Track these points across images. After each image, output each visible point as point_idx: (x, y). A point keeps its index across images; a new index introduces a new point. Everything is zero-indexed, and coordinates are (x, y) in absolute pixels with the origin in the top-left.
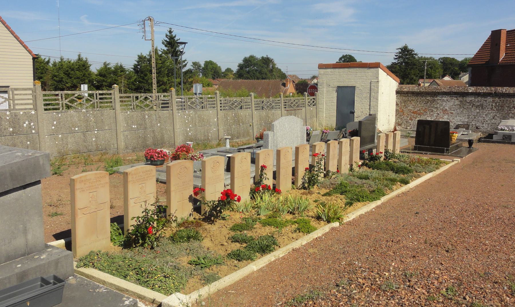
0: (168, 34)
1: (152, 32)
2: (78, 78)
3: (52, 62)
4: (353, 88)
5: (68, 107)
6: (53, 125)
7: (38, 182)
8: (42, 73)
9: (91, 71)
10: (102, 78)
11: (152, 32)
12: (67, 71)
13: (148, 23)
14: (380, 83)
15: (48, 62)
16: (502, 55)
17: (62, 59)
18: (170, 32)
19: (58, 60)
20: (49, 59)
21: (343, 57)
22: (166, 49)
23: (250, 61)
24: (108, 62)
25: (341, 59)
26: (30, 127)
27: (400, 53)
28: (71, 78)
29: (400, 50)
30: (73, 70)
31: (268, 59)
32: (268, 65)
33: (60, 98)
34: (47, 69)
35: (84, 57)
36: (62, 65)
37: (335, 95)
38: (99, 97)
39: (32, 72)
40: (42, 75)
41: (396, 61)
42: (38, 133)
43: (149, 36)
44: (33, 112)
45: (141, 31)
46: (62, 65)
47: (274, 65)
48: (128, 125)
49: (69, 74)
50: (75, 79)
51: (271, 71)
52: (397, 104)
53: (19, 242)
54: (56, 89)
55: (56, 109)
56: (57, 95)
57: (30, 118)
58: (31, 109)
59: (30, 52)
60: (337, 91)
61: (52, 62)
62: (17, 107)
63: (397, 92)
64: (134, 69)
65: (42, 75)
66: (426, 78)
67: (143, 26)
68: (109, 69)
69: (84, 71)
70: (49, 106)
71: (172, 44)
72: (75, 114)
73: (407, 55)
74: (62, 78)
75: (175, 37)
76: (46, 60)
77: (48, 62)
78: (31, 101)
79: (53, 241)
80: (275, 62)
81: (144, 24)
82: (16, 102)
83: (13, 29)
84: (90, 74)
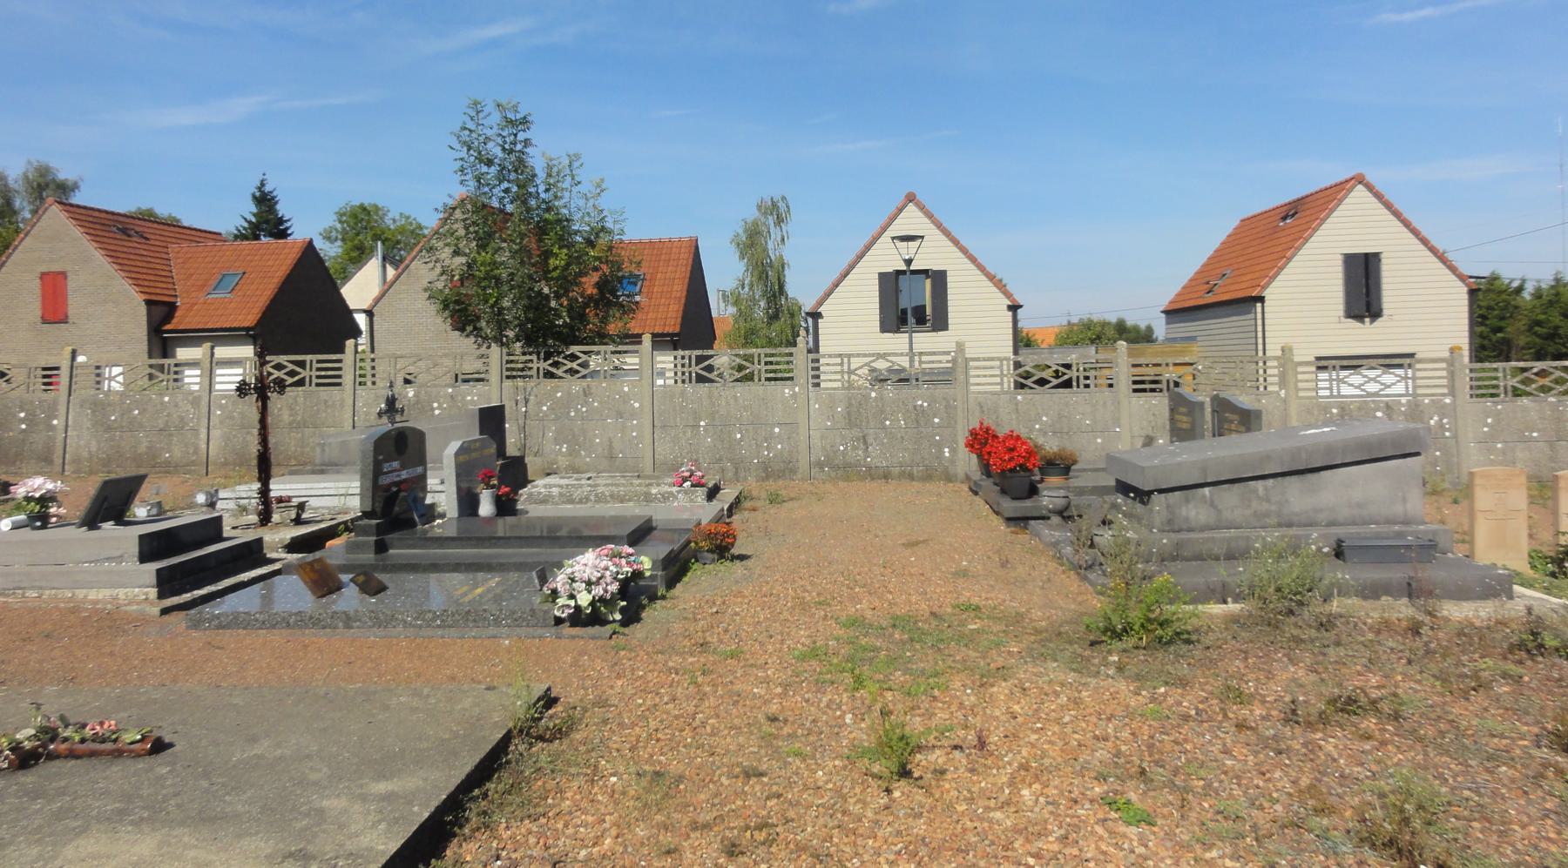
3: (1530, 288)
5: (1517, 393)
6: (1487, 425)
7: (1417, 454)
8: (1502, 318)
15: (1520, 290)
20: (1524, 281)
26: (1441, 426)
33: (1500, 375)
34: (1516, 307)
36: (1557, 294)
38: (315, 365)
39: (1466, 321)
40: (1502, 324)
42: (1455, 436)
44: (1448, 401)
46: (1557, 294)
53: (1398, 509)
54: (1539, 357)
55: (1493, 395)
56: (1496, 370)
57: (1443, 411)
58: (1444, 395)
59: (1462, 278)
61: (1530, 288)
62: (1420, 391)
65: (1502, 324)
70: (1485, 390)
72: (1532, 405)
74: (1557, 328)
76: (1515, 284)
77: (1520, 290)
78: (1444, 382)
82: (1419, 382)
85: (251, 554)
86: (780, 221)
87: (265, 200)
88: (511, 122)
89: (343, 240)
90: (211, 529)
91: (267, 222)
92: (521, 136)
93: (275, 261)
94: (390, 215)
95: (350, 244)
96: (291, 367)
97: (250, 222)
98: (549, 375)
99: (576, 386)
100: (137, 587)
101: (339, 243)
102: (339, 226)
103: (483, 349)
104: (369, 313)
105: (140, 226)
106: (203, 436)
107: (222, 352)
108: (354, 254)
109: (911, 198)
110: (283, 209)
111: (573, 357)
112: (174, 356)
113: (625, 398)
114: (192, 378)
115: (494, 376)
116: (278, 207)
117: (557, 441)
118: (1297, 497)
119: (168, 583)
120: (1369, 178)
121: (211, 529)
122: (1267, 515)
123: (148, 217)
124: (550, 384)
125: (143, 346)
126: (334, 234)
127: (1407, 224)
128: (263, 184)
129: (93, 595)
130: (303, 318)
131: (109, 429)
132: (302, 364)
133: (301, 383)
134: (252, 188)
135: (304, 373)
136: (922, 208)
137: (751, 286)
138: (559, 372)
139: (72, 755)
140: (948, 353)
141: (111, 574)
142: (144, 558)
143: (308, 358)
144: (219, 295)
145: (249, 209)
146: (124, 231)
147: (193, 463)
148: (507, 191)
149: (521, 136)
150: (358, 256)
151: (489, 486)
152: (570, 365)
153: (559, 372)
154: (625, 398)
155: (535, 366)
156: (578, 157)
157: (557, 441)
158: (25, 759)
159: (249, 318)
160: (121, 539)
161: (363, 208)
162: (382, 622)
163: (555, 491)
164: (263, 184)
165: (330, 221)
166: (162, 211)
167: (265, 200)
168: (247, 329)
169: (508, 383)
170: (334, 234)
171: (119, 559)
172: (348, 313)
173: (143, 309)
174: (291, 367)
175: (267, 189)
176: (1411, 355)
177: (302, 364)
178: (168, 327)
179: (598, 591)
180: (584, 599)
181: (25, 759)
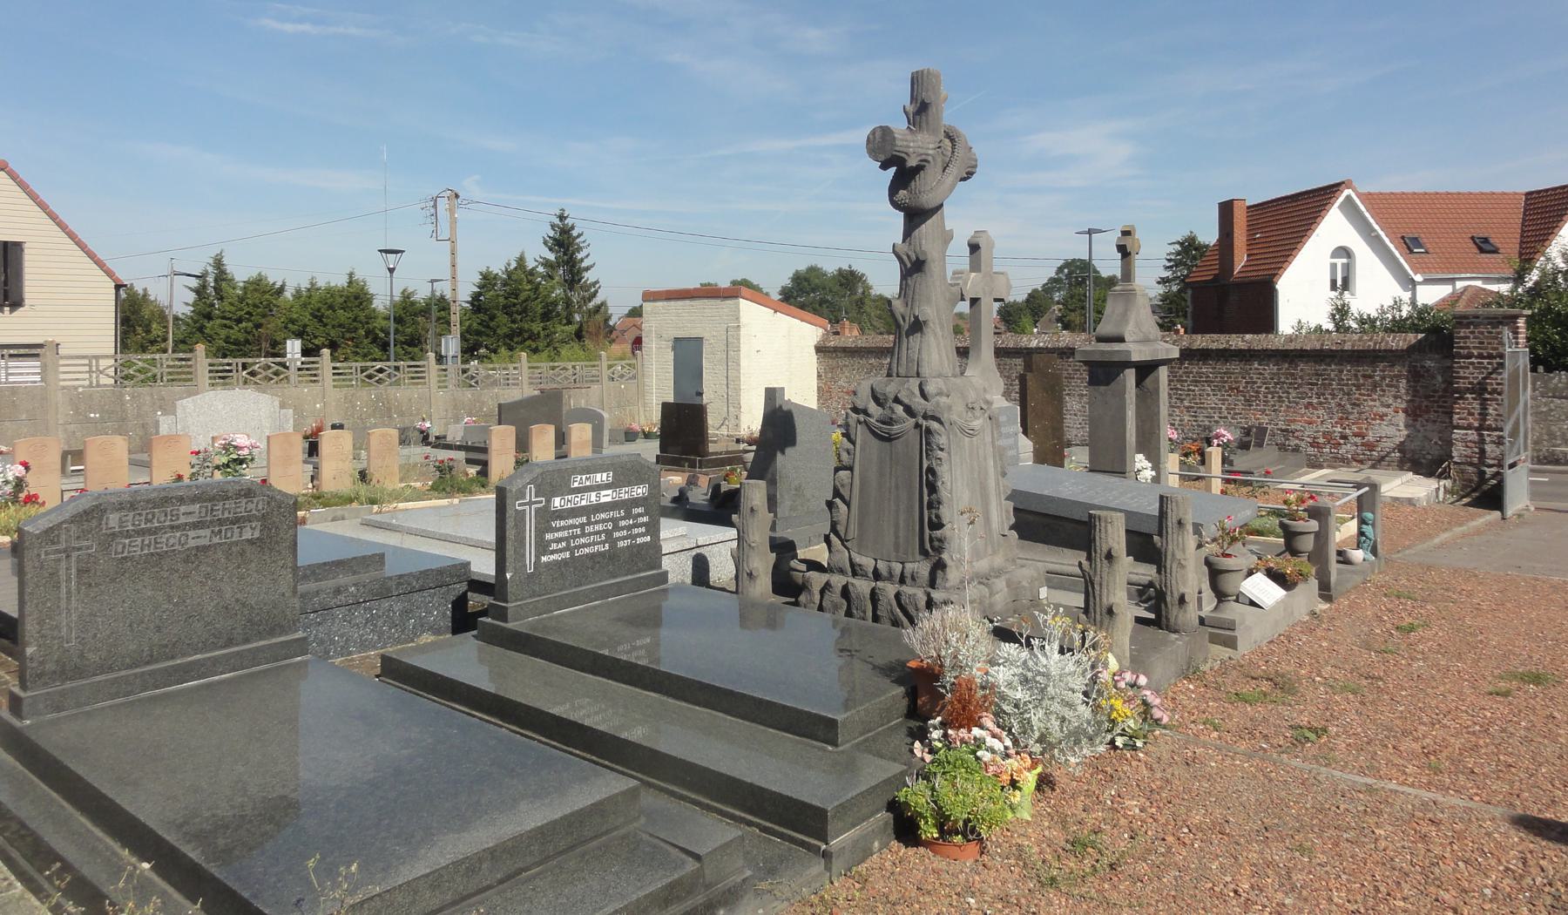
0: (557, 221)
1: (454, 222)
2: (340, 326)
4: (699, 340)
8: (264, 316)
11: (454, 222)
13: (443, 205)
14: (743, 331)
15: (281, 290)
16: (1240, 261)
18: (562, 218)
19: (305, 285)
21: (1068, 264)
22: (552, 257)
23: (806, 280)
24: (410, 290)
25: (1060, 270)
27: (1178, 253)
29: (1178, 247)
30: (331, 307)
31: (852, 273)
32: (853, 291)
35: (358, 276)
37: (671, 356)
40: (263, 321)
41: (1168, 274)
43: (445, 233)
47: (868, 288)
48: (77, 412)
51: (860, 303)
52: (819, 376)
59: (110, 273)
60: (674, 349)
63: (820, 349)
64: (472, 303)
65: (263, 321)
68: (413, 304)
69: (356, 310)
71: (564, 242)
73: (1194, 258)
74: (305, 326)
75: (573, 228)
77: (281, 290)
80: (870, 282)
81: (435, 206)
84: (372, 316)
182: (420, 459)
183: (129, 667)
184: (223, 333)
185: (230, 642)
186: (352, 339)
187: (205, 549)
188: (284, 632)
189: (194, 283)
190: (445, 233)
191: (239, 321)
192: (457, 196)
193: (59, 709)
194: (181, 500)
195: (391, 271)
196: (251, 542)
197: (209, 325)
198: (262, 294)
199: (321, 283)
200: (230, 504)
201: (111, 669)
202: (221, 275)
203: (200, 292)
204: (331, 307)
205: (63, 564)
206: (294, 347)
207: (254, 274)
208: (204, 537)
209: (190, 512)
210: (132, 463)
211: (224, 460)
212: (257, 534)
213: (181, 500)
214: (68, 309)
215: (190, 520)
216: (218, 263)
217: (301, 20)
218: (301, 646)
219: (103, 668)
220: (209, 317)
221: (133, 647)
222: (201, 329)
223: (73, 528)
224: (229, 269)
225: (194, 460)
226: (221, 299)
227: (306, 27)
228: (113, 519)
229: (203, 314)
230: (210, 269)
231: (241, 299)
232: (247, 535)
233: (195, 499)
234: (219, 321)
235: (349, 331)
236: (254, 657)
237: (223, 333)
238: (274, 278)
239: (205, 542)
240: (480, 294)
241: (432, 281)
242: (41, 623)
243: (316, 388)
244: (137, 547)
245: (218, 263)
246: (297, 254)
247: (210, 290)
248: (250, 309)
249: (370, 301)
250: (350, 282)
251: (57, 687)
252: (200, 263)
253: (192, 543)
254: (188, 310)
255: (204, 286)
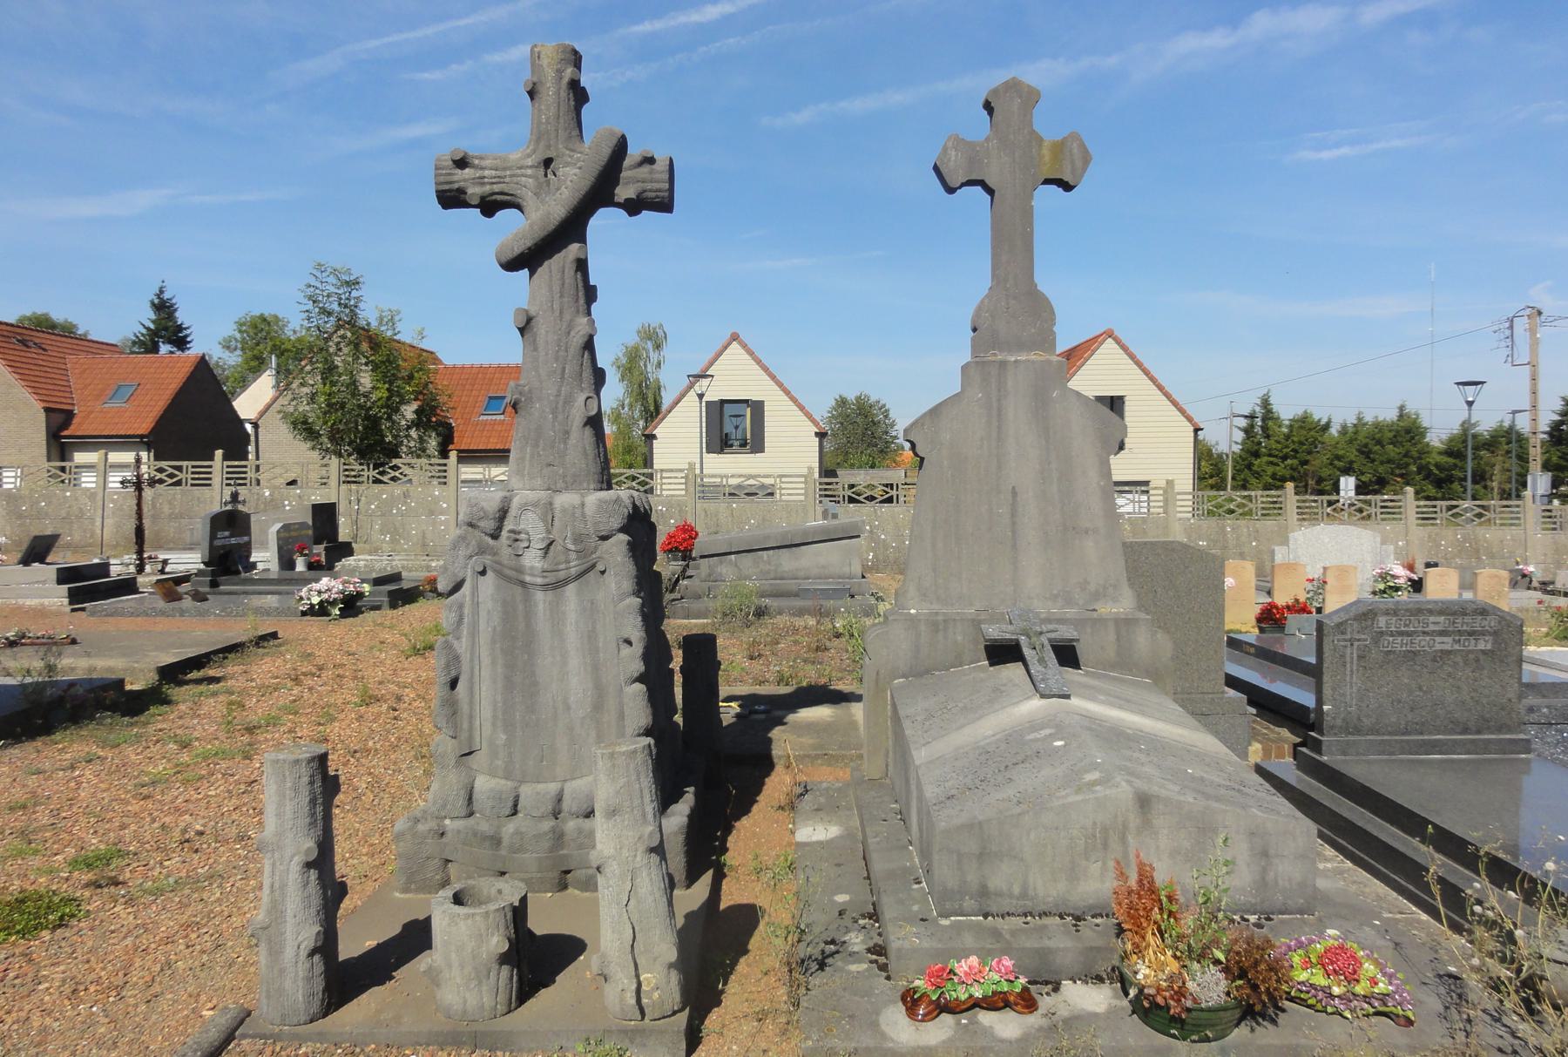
1: (1534, 344)
2: (1389, 461)
8: (1310, 453)
9: (1428, 445)
10: (1451, 460)
12: (1366, 445)
13: (1521, 325)
15: (1327, 426)
17: (1360, 419)
19: (1351, 420)
28: (1373, 461)
30: (1379, 442)
35: (1411, 408)
45: (1503, 344)
49: (1370, 451)
50: (1382, 463)
53: (846, 570)
59: (1189, 419)
64: (1549, 433)
66: (1234, 488)
67: (1508, 333)
74: (1351, 462)
76: (1323, 422)
77: (1327, 426)
79: (1029, 698)
81: (1511, 327)
83: (1161, 381)
84: (1426, 450)
85: (127, 586)
86: (658, 347)
87: (163, 308)
88: (347, 283)
89: (243, 349)
90: (103, 569)
91: (166, 329)
92: (354, 294)
93: (171, 368)
94: (291, 326)
95: (249, 354)
96: (171, 470)
97: (148, 329)
98: (377, 481)
99: (397, 489)
100: (58, 598)
101: (239, 352)
102: (238, 336)
103: (326, 461)
104: (256, 426)
105: (40, 338)
106: (98, 523)
107: (116, 457)
108: (253, 364)
109: (735, 337)
110: (182, 317)
111: (395, 468)
112: (71, 460)
113: (436, 500)
114: (88, 480)
115: (333, 482)
116: (177, 314)
117: (382, 532)
118: (787, 562)
119: (76, 597)
120: (1116, 333)
121: (103, 569)
122: (768, 572)
123: (44, 325)
124: (377, 488)
125: (42, 450)
126: (233, 343)
127: (1146, 373)
128: (161, 292)
129: (29, 602)
130: (197, 424)
131: (20, 516)
132: (179, 469)
133: (179, 483)
134: (151, 295)
135: (181, 476)
136: (744, 346)
137: (631, 406)
138: (385, 479)
139: (32, 644)
140: (681, 471)
141: (41, 592)
142: (60, 581)
143: (184, 464)
144: (116, 404)
145: (148, 316)
146: (23, 342)
147: (90, 545)
148: (343, 337)
149: (354, 294)
150: (256, 366)
151: (302, 555)
152: (393, 474)
153: (385, 479)
154: (436, 500)
155: (366, 473)
156: (399, 312)
157: (382, 532)
158: (12, 644)
159: (144, 426)
160: (44, 573)
161: (263, 319)
162: (202, 614)
163: (362, 563)
164: (161, 292)
165: (230, 330)
166: (58, 316)
167: (163, 308)
168: (142, 436)
169: (344, 487)
170: (233, 343)
171: (44, 582)
172: (241, 422)
173: (42, 416)
174: (171, 470)
175: (166, 296)
176: (1146, 483)
177: (179, 469)
178: (65, 433)
179: (325, 596)
180: (316, 600)
181: (12, 644)
182: (1533, 603)
183: (1390, 734)
184: (1270, 470)
185: (1465, 731)
186: (1401, 476)
187: (1449, 652)
188: (1510, 731)
189: (1243, 423)
190: (1523, 355)
191: (1285, 458)
192: (1540, 313)
193: (1344, 753)
194: (1431, 612)
195: (1470, 404)
196: (1483, 652)
197: (1256, 462)
198: (1309, 431)
199: (1369, 418)
200: (1468, 619)
201: (1378, 733)
202: (1268, 414)
203: (1248, 431)
204: (1379, 442)
205: (1348, 651)
206: (1348, 484)
207: (1300, 412)
208: (1446, 643)
209: (1437, 622)
210: (1258, 589)
211: (1382, 586)
212: (1489, 647)
213: (1431, 612)
214: (1159, 453)
215: (1437, 628)
216: (1266, 403)
217: (1338, 145)
218: (1526, 746)
219: (1373, 731)
220: (1256, 455)
221: (1393, 720)
222: (1249, 466)
223: (1356, 625)
224: (1275, 408)
225: (1309, 586)
226: (1268, 437)
227: (1344, 151)
228: (1382, 621)
229: (1251, 452)
230: (1258, 409)
231: (1287, 437)
232: (1481, 646)
233: (1441, 613)
234: (1265, 459)
235: (1399, 466)
236: (1486, 747)
237: (1270, 470)
238: (1320, 415)
239: (1447, 647)
240: (1562, 423)
241: (1514, 412)
242: (1334, 689)
243: (1400, 526)
244: (1399, 644)
245: (1266, 403)
246: (1341, 391)
247: (1258, 430)
248: (1296, 446)
249: (1423, 435)
250: (1401, 416)
251: (1343, 738)
252: (1249, 404)
253: (1438, 647)
254: (1237, 448)
255: (1252, 426)
